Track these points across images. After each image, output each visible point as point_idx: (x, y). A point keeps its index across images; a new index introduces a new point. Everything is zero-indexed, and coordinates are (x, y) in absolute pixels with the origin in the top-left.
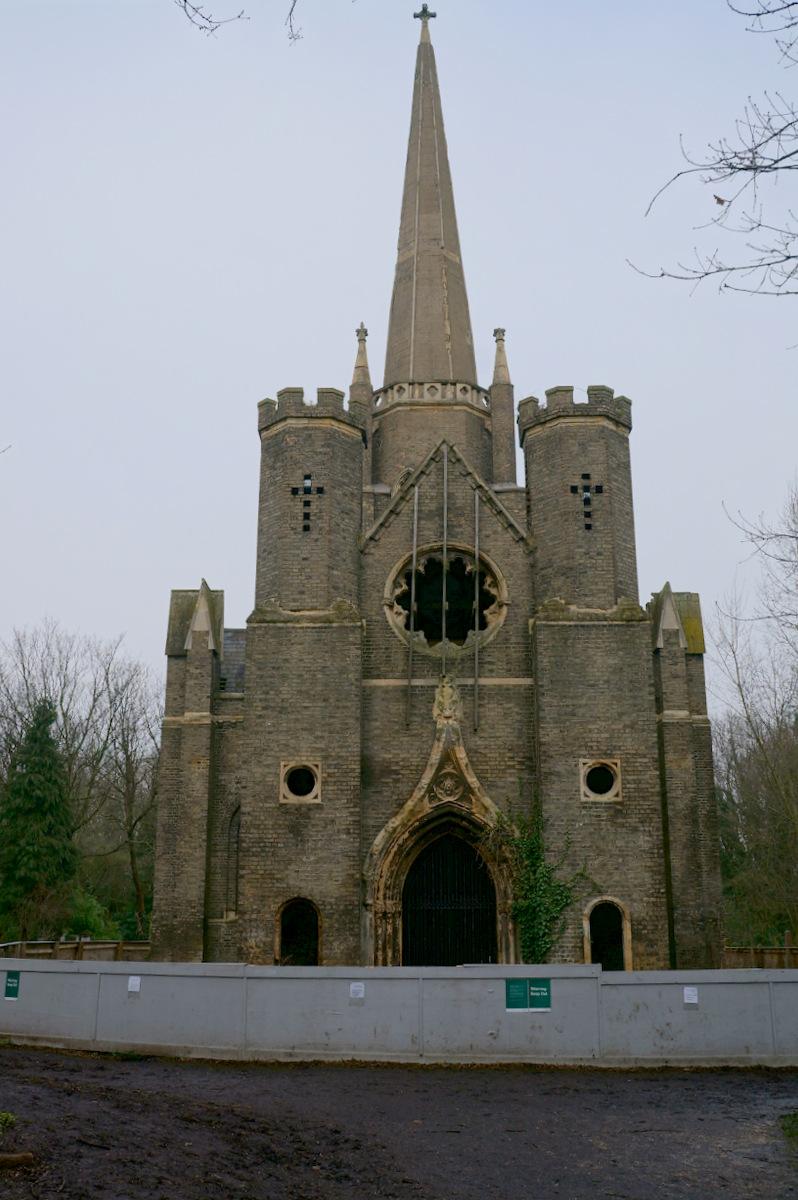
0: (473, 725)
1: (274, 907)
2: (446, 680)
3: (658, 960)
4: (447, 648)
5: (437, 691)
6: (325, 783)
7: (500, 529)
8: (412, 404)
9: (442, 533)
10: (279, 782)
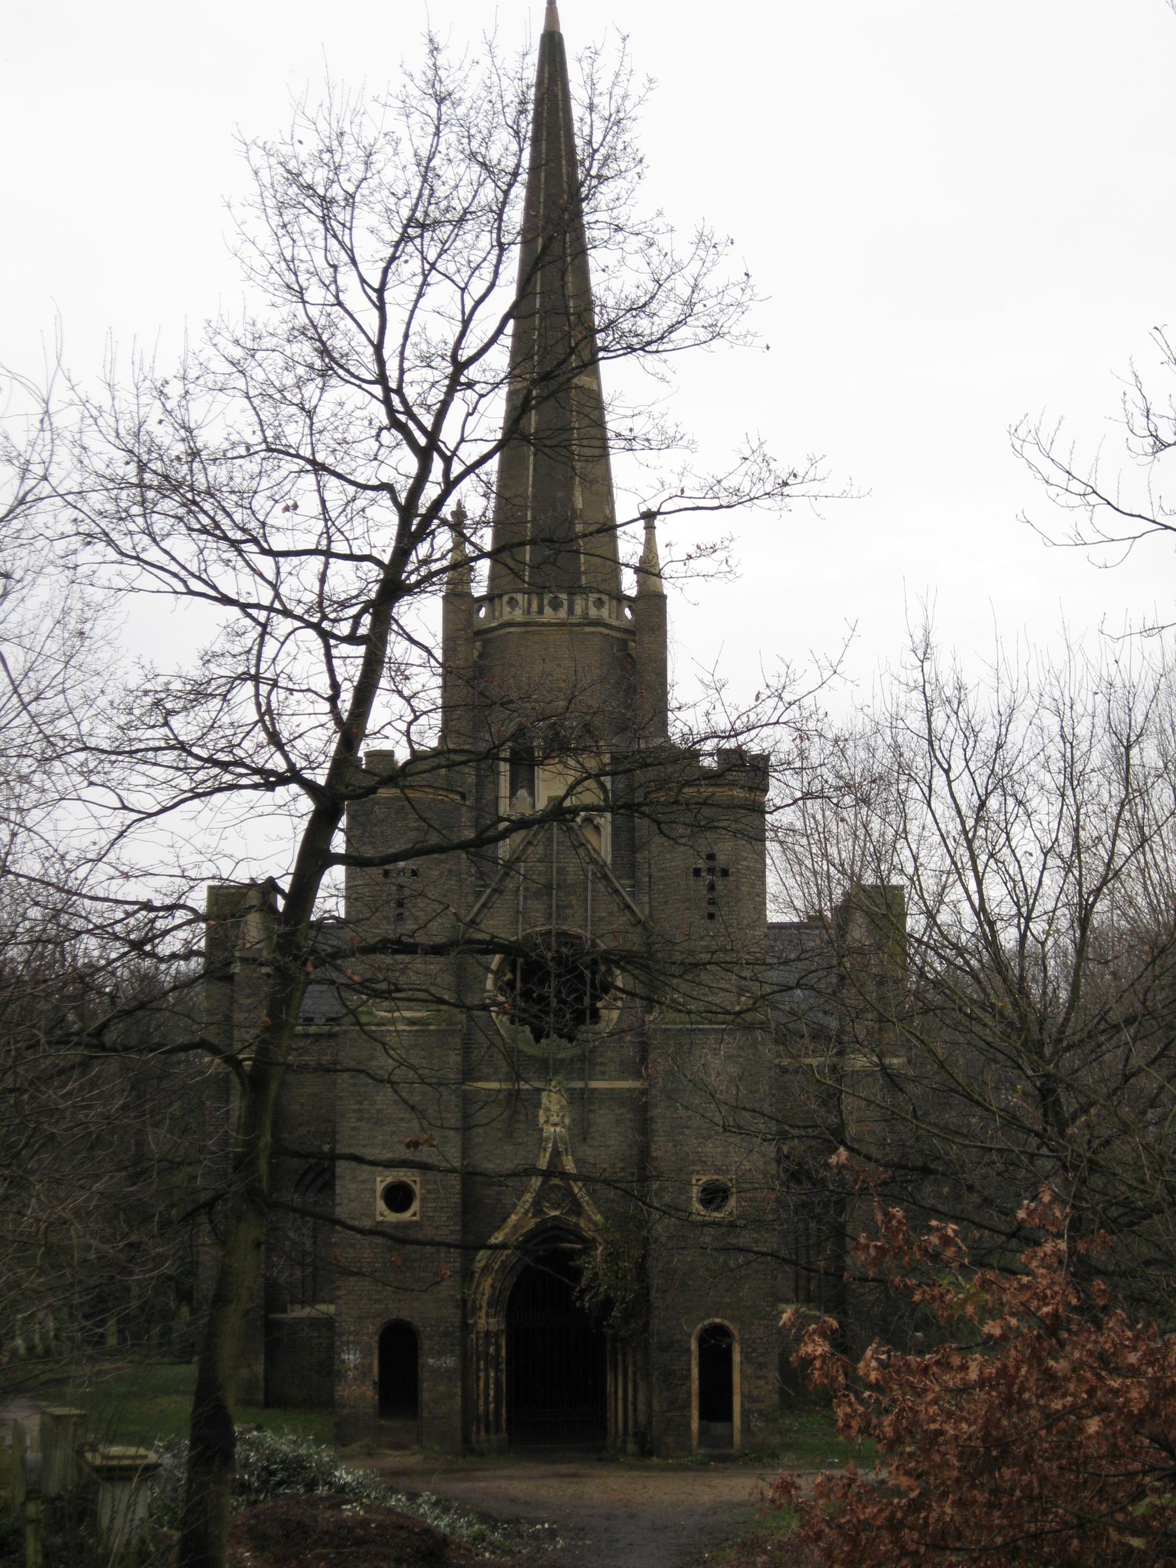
0: (582, 1131)
1: (371, 1329)
2: (553, 1083)
3: (767, 1383)
4: (557, 1048)
5: (544, 1094)
6: (424, 1200)
7: (616, 909)
8: (526, 624)
9: (550, 915)
10: (375, 1199)
